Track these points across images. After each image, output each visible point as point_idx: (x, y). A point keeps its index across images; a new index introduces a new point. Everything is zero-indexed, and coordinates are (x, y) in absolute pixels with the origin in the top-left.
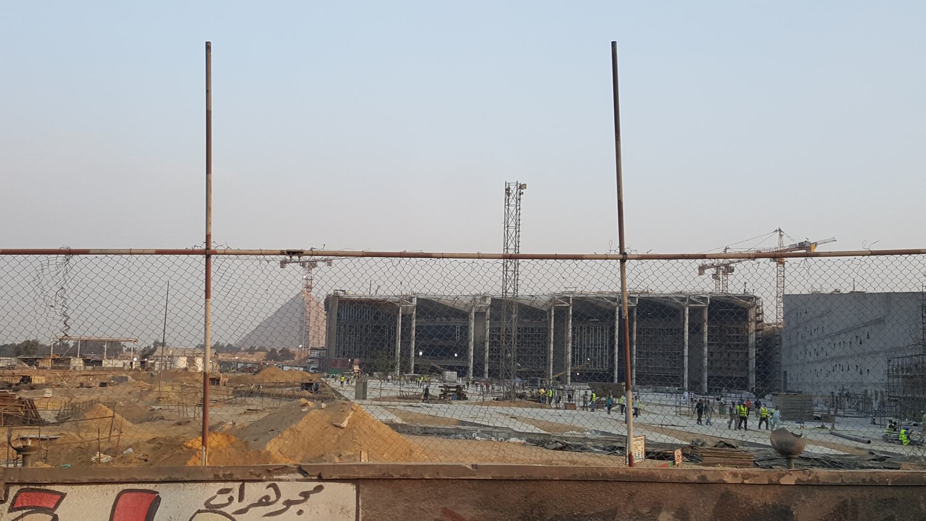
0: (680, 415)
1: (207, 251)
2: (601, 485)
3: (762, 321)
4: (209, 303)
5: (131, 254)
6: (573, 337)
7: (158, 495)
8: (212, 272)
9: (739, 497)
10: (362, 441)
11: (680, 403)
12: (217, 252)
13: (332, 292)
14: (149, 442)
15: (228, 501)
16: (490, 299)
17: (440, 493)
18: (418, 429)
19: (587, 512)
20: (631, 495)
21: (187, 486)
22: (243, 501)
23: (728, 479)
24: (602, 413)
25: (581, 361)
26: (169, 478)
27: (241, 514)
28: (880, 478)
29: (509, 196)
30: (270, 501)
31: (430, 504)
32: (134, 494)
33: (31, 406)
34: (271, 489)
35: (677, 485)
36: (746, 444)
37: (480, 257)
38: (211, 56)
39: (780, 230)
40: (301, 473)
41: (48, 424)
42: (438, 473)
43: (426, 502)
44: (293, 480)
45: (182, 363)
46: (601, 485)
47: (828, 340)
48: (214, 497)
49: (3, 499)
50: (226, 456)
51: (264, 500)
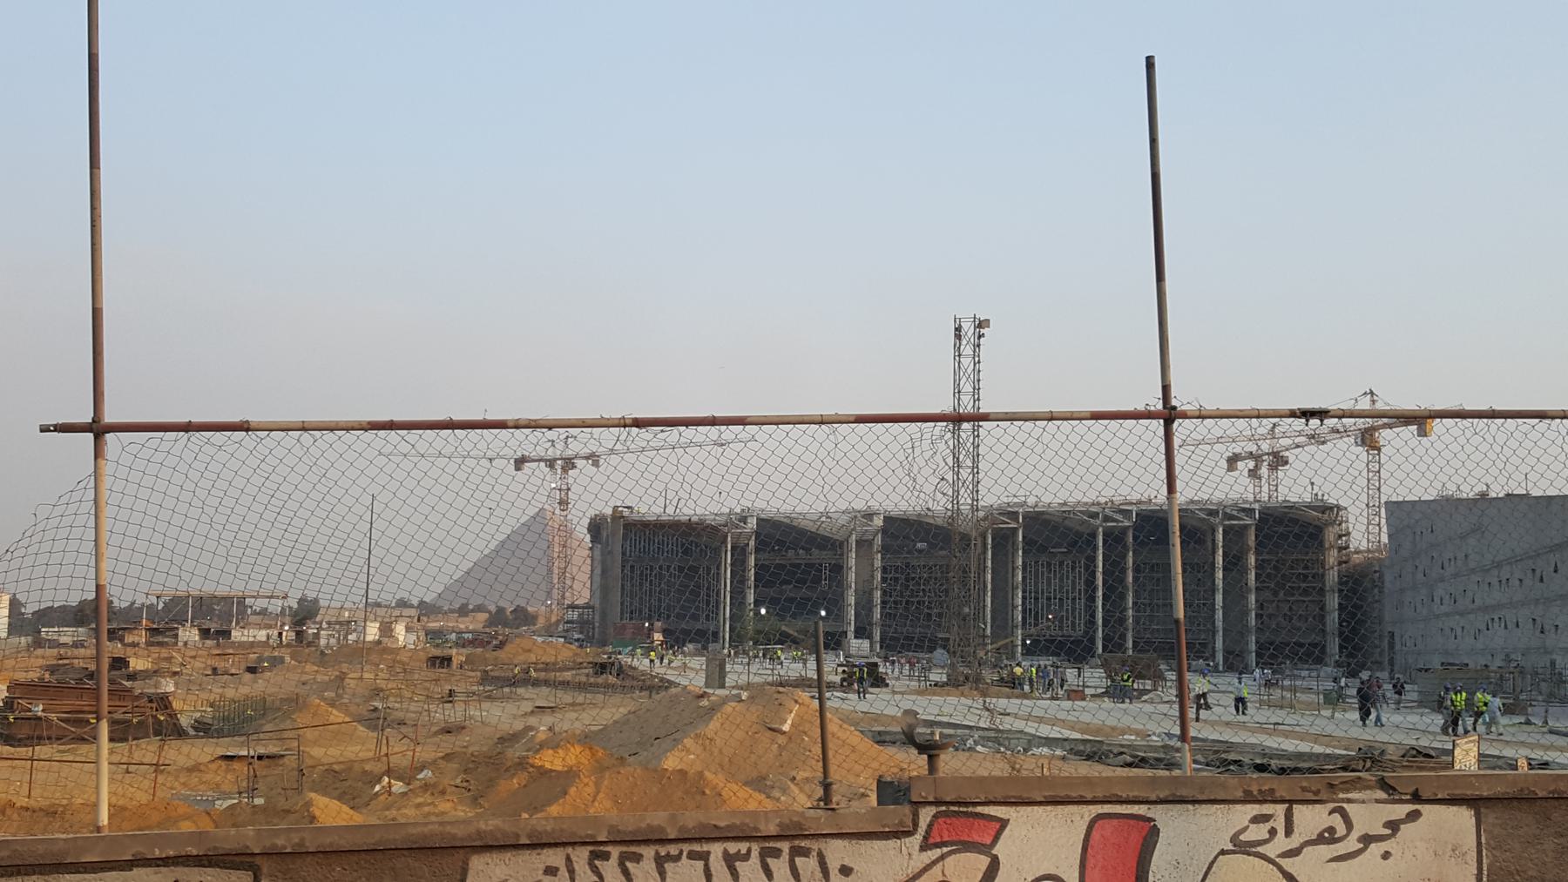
7: (1155, 825)
15: (1267, 836)
16: (882, 518)
22: (1293, 836)
25: (1036, 618)
26: (1171, 795)
30: (1336, 836)
32: (1115, 822)
34: (1337, 816)
37: (1493, 415)
39: (1372, 393)
40: (1382, 788)
44: (1370, 801)
45: (372, 632)
47: (1475, 578)
48: (1246, 829)
49: (911, 829)
50: (628, 779)
51: (1326, 835)
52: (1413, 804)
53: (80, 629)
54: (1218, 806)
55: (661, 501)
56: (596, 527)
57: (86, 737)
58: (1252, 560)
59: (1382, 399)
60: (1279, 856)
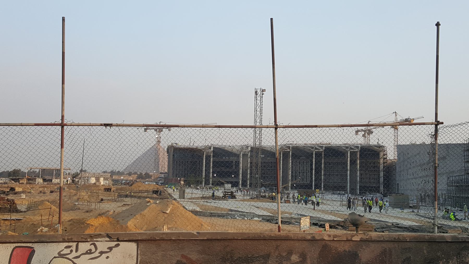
0: (342, 205)
1: (62, 124)
2: (262, 241)
3: (386, 158)
4: (63, 151)
5: (21, 125)
6: (292, 167)
8: (64, 135)
9: (332, 247)
10: (177, 220)
11: (342, 200)
12: (67, 124)
13: (170, 144)
14: (69, 221)
15: (70, 252)
17: (180, 247)
18: (208, 214)
19: (255, 255)
20: (277, 247)
21: (49, 245)
22: (78, 252)
23: (326, 238)
24: (302, 205)
27: (76, 258)
28: (403, 238)
29: (257, 95)
30: (92, 252)
31: (175, 252)
33: (13, 202)
34: (93, 246)
35: (301, 241)
36: (372, 220)
38: (65, 24)
39: (396, 113)
41: (21, 212)
42: (179, 237)
43: (173, 251)
44: (104, 241)
45: (93, 180)
46: (262, 241)
51: (89, 252)
52: (118, 242)
54: (55, 243)
55: (189, 141)
58: (358, 162)
60: (73, 258)
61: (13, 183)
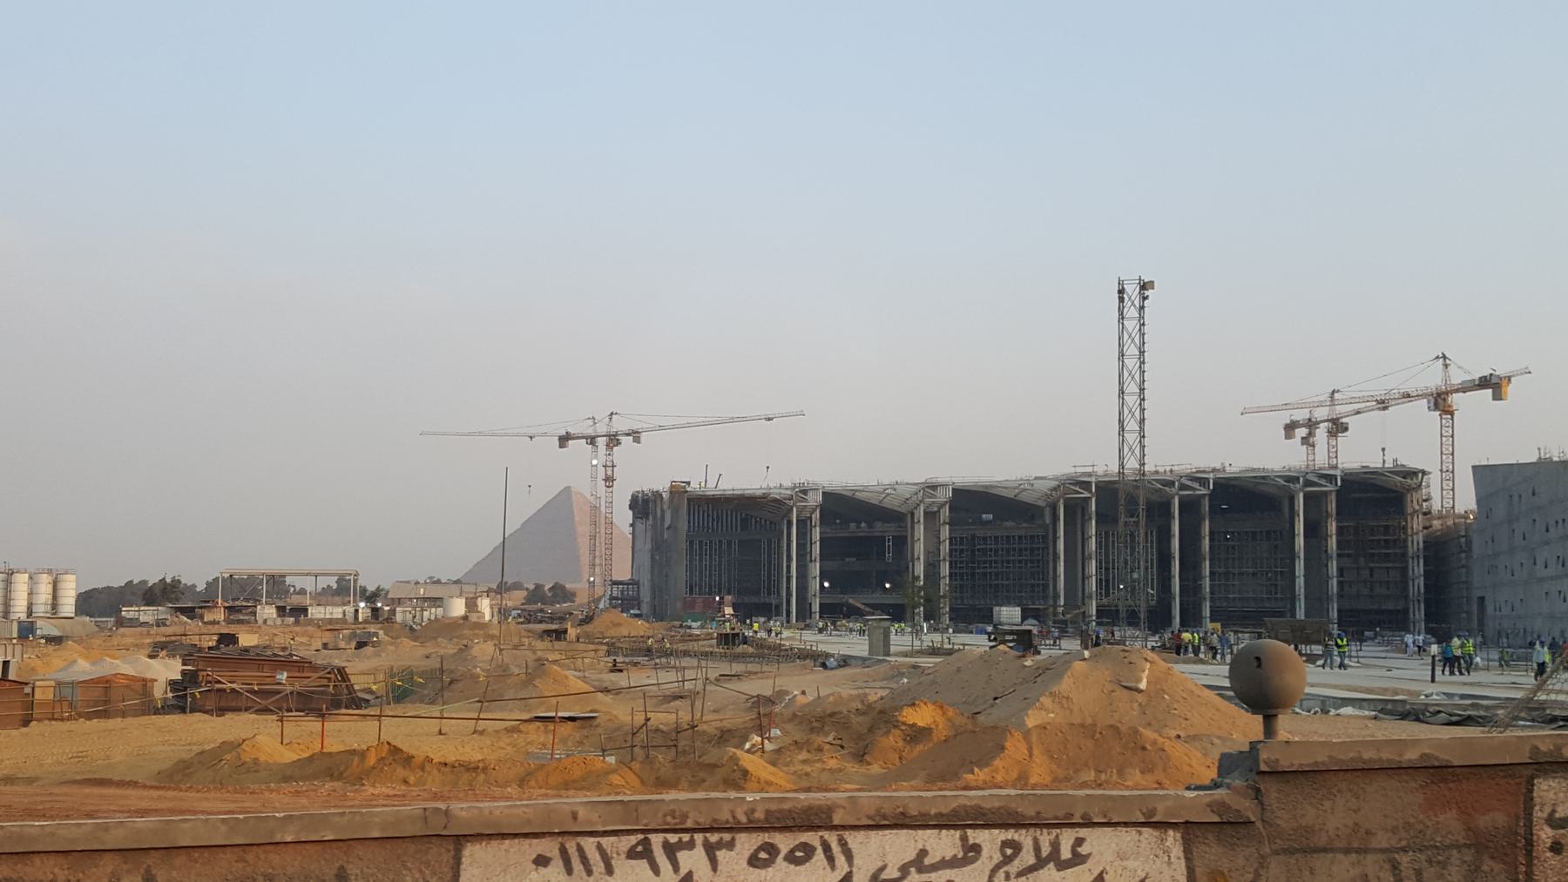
10: (1187, 713)
39: (1444, 357)
45: (458, 608)
53: (160, 608)
56: (642, 506)
57: (272, 708)
59: (1454, 363)
61: (186, 623)
